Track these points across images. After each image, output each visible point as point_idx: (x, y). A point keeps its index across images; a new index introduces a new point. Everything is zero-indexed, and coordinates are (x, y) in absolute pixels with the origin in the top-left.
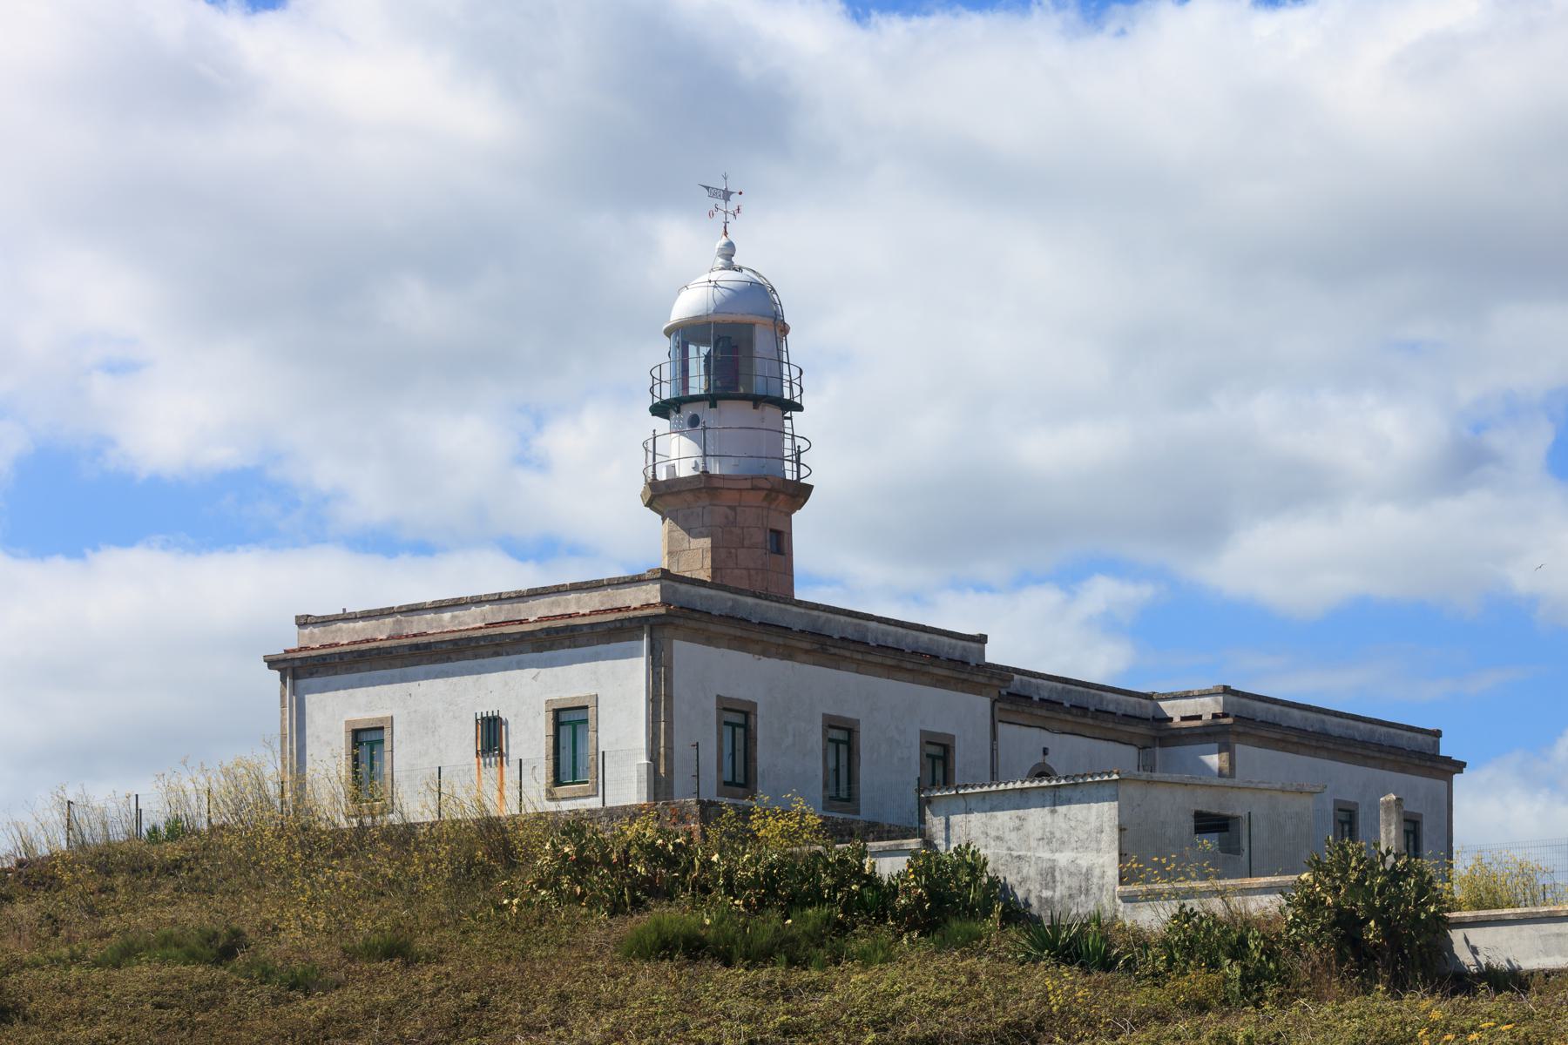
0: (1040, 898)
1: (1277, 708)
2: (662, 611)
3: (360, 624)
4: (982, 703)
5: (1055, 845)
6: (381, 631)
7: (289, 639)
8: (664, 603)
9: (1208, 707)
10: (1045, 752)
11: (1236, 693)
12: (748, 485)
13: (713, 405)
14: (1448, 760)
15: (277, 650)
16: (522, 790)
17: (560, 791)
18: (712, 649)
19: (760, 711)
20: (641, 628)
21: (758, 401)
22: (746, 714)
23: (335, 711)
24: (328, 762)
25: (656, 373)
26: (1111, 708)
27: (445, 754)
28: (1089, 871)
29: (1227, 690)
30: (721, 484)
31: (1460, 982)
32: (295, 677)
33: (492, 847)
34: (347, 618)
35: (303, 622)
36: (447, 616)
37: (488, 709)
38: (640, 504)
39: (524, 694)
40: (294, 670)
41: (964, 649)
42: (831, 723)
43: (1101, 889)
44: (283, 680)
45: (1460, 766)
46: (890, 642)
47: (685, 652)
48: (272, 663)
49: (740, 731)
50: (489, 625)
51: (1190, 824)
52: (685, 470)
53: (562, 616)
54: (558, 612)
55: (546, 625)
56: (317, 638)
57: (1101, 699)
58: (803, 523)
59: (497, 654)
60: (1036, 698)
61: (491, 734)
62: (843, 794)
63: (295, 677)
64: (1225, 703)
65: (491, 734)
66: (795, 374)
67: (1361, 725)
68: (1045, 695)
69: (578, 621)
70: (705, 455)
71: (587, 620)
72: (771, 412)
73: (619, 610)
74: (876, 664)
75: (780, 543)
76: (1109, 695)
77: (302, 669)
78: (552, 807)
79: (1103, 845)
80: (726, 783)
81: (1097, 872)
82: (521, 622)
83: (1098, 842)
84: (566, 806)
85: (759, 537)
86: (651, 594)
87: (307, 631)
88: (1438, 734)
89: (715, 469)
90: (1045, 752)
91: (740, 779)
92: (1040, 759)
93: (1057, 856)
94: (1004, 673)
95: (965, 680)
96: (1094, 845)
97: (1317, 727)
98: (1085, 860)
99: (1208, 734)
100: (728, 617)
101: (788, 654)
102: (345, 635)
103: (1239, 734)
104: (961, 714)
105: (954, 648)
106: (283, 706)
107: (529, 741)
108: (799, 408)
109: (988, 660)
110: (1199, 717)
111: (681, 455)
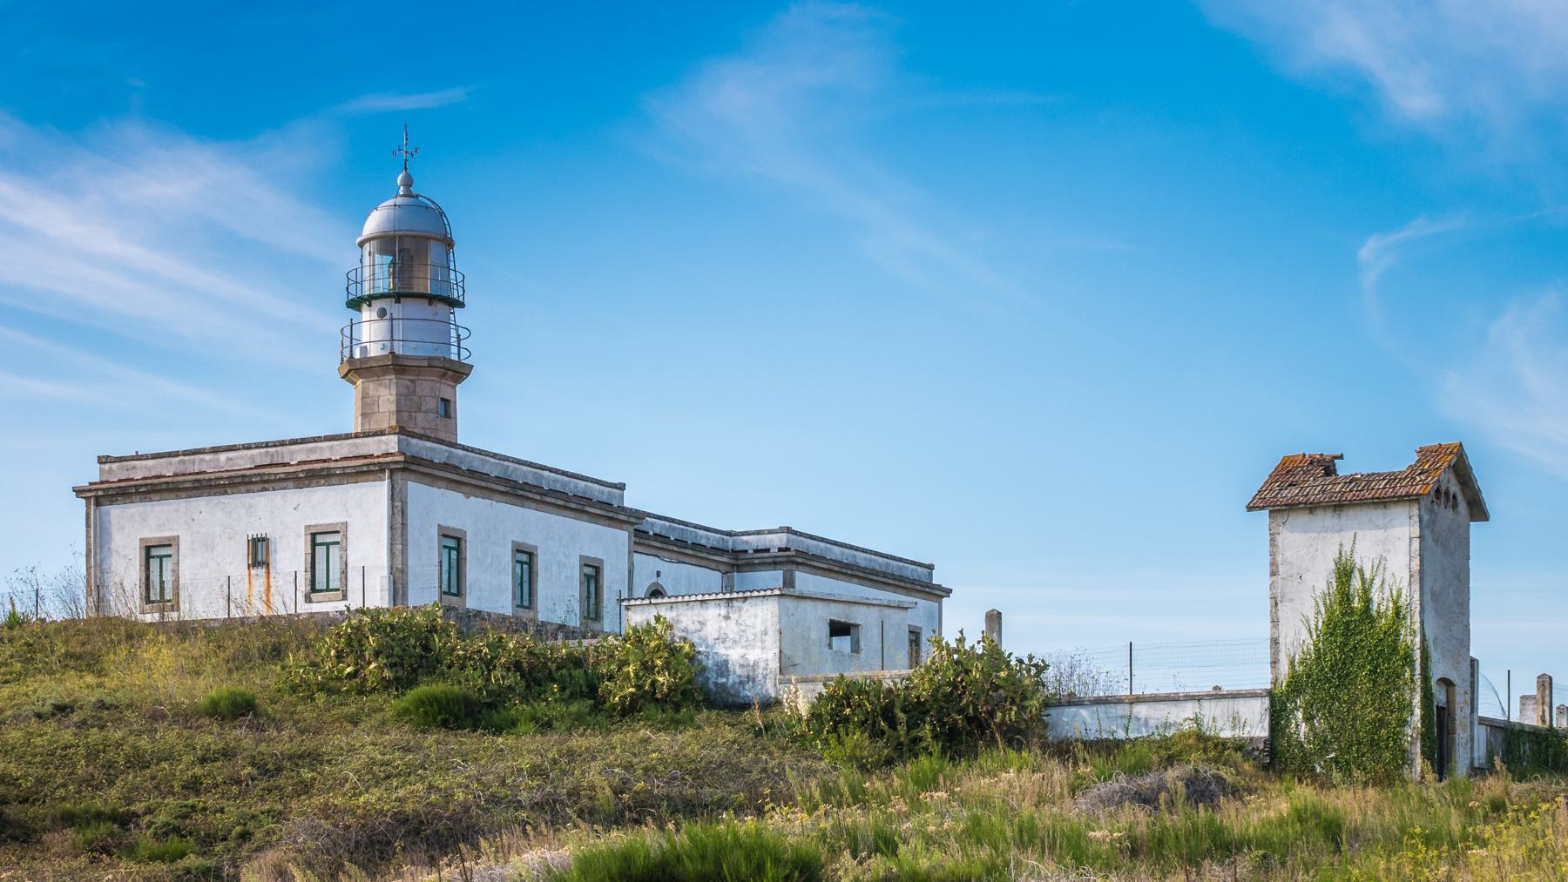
0: (716, 684)
1: (822, 545)
2: (401, 458)
3: (150, 463)
4: (622, 536)
5: (728, 644)
6: (167, 468)
7: (91, 474)
8: (401, 453)
9: (778, 541)
10: (658, 574)
11: (795, 533)
12: (425, 363)
13: (398, 301)
14: (939, 587)
16: (285, 595)
17: (314, 596)
19: (468, 538)
20: (382, 471)
21: (431, 299)
22: (458, 540)
23: (133, 525)
24: (126, 570)
25: (352, 276)
26: (703, 542)
27: (218, 566)
28: (756, 664)
29: (789, 530)
31: (1063, 750)
32: (98, 504)
33: (272, 639)
34: (138, 457)
35: (103, 460)
36: (223, 457)
38: (338, 376)
39: (286, 516)
40: (97, 498)
42: (518, 549)
43: (765, 677)
44: (88, 506)
45: (948, 592)
46: (558, 487)
47: (416, 490)
48: (79, 492)
49: (454, 554)
50: (257, 467)
51: (827, 630)
52: (375, 351)
53: (317, 461)
55: (306, 467)
56: (117, 472)
58: (465, 397)
59: (265, 489)
61: (259, 552)
62: (526, 603)
63: (98, 504)
65: (259, 552)
66: (460, 278)
67: (880, 559)
68: (657, 531)
69: (333, 465)
70: (392, 340)
71: (340, 464)
73: (365, 457)
75: (447, 408)
76: (702, 532)
77: (100, 496)
78: (304, 608)
81: (762, 665)
82: (285, 465)
83: (763, 641)
84: (316, 608)
85: (432, 404)
87: (107, 467)
88: (931, 567)
89: (399, 351)
90: (658, 574)
93: (730, 652)
94: (640, 515)
95: (610, 518)
97: (850, 560)
98: (753, 655)
99: (775, 563)
102: (140, 471)
104: (609, 544)
106: (88, 526)
107: (290, 558)
108: (462, 305)
109: (626, 505)
110: (768, 550)
111: (371, 333)
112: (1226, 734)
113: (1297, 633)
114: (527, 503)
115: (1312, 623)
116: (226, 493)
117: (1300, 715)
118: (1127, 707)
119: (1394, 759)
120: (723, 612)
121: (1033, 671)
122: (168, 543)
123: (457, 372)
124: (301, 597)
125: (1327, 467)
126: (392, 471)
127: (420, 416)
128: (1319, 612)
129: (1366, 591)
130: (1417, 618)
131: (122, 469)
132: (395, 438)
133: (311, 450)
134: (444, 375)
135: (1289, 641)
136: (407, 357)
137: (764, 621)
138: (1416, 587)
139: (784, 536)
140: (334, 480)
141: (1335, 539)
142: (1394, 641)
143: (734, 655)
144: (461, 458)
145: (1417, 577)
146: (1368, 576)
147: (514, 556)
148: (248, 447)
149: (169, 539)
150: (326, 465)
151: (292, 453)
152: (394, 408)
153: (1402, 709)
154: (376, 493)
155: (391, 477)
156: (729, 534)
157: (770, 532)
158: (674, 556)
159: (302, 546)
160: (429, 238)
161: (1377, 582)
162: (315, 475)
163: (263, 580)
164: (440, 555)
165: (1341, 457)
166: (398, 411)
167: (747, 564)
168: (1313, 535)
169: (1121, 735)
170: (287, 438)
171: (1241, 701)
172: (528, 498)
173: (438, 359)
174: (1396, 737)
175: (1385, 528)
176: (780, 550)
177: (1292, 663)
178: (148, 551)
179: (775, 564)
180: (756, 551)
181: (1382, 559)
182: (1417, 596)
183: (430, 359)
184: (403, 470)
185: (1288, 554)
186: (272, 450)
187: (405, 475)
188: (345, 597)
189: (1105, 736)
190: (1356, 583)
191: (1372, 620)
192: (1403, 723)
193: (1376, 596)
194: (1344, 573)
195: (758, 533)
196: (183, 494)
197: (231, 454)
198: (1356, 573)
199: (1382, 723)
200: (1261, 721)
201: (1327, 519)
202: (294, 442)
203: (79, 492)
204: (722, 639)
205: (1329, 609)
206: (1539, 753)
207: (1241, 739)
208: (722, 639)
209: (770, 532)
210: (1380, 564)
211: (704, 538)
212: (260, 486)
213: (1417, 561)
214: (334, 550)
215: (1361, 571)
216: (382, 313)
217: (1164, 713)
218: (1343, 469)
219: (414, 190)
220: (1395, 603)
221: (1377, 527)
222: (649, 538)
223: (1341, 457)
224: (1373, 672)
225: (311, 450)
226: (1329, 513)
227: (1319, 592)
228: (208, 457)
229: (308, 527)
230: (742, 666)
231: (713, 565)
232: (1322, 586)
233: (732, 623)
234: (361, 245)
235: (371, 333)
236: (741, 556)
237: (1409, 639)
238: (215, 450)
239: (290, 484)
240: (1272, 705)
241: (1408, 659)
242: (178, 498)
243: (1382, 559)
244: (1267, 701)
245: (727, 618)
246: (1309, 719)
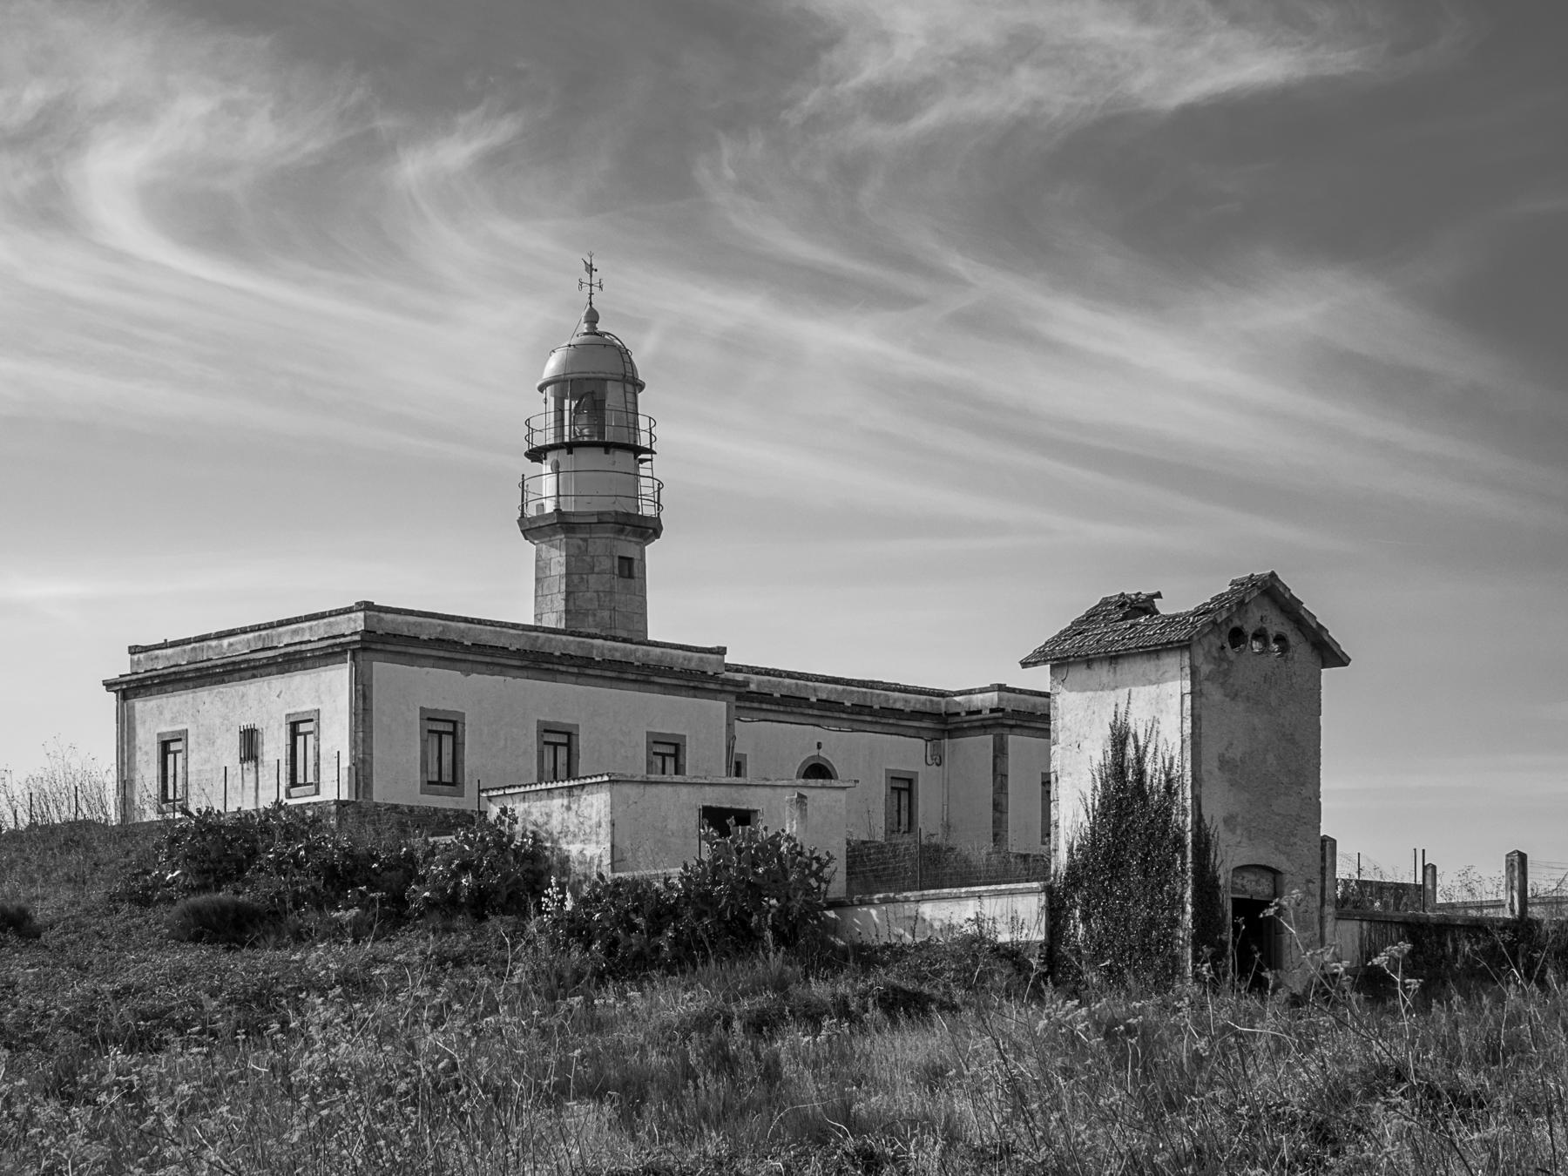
4: (719, 707)
5: (570, 838)
6: (179, 657)
7: (122, 666)
10: (819, 746)
13: (570, 452)
15: (113, 675)
16: (251, 793)
17: (294, 791)
18: (416, 668)
20: (345, 652)
22: (455, 723)
26: (899, 706)
30: (573, 520)
35: (134, 650)
36: (225, 642)
37: (246, 724)
39: (268, 702)
41: (701, 659)
47: (382, 670)
48: (109, 685)
54: (297, 640)
56: (146, 664)
57: (887, 698)
58: (655, 555)
59: (254, 676)
60: (813, 699)
61: (250, 743)
64: (1000, 699)
65: (250, 743)
70: (558, 495)
72: (623, 459)
74: (597, 677)
75: (630, 570)
77: (128, 690)
79: (601, 838)
80: (430, 783)
86: (358, 622)
87: (136, 657)
90: (819, 746)
91: (447, 778)
92: (815, 752)
93: (571, 847)
95: (694, 688)
96: (594, 838)
98: (591, 850)
99: (985, 727)
100: (438, 640)
101: (502, 669)
103: (1012, 727)
105: (690, 660)
110: (979, 712)
111: (546, 487)
112: (1004, 938)
113: (1075, 815)
114: (559, 677)
115: (1089, 801)
116: (223, 682)
117: (1078, 913)
118: (913, 906)
119: (1165, 967)
120: (565, 802)
121: (815, 866)
122: (181, 737)
123: (649, 529)
124: (282, 790)
125: (1142, 607)
126: (354, 652)
127: (592, 578)
128: (1095, 788)
129: (1140, 760)
130: (1188, 794)
131: (146, 659)
132: (361, 615)
133: (295, 632)
134: (621, 531)
135: (1068, 824)
136: (573, 514)
137: (599, 812)
138: (1188, 755)
139: (994, 695)
140: (309, 663)
141: (1110, 697)
142: (1166, 822)
143: (573, 849)
144: (462, 633)
145: (1188, 742)
146: (1141, 743)
147: (540, 737)
148: (244, 631)
149: (179, 732)
150: (298, 648)
151: (280, 635)
152: (563, 570)
153: (1172, 907)
154: (337, 681)
155: (353, 658)
156: (942, 694)
157: (982, 691)
158: (847, 724)
159: (283, 736)
160: (605, 380)
161: (1151, 749)
162: (292, 661)
163: (253, 775)
164: (424, 742)
165: (1158, 595)
166: (568, 574)
167: (957, 729)
168: (1089, 694)
169: (908, 938)
170: (275, 619)
171: (1020, 898)
172: (558, 671)
173: (608, 513)
174: (1168, 940)
175: (1158, 682)
176: (992, 711)
177: (1070, 850)
178: (165, 747)
179: (984, 727)
180: (969, 713)
181: (1155, 721)
182: (1188, 766)
183: (599, 514)
184: (364, 649)
185: (1067, 718)
186: (263, 633)
187: (370, 655)
188: (317, 792)
189: (894, 941)
190: (1131, 752)
191: (1145, 798)
192: (1175, 923)
193: (1149, 769)
194: (1120, 738)
195: (970, 692)
196: (190, 684)
197: (232, 639)
198: (1131, 740)
199: (1152, 923)
200: (1038, 921)
201: (1102, 672)
202: (281, 624)
203: (109, 685)
204: (565, 833)
205: (1105, 784)
206: (1436, 949)
207: (1018, 943)
208: (565, 833)
209: (982, 691)
210: (1152, 730)
211: (898, 701)
212: (249, 673)
213: (1188, 724)
214: (310, 738)
215: (1136, 741)
216: (556, 469)
217: (947, 913)
218: (1164, 607)
219: (600, 327)
220: (1167, 775)
221: (1151, 683)
222: (811, 706)
223: (1158, 595)
224: (1144, 860)
225: (295, 632)
226: (1106, 667)
227: (1095, 766)
228: (214, 643)
229: (288, 716)
230: (580, 863)
231: (911, 732)
232: (1098, 757)
233: (572, 814)
234: (541, 388)
235: (546, 487)
236: (951, 720)
237: (1180, 818)
238: (220, 636)
239: (274, 669)
240: (1050, 901)
241: (1179, 842)
242: (187, 688)
243: (1155, 721)
244: (1043, 897)
245: (569, 808)
246: (1085, 918)
